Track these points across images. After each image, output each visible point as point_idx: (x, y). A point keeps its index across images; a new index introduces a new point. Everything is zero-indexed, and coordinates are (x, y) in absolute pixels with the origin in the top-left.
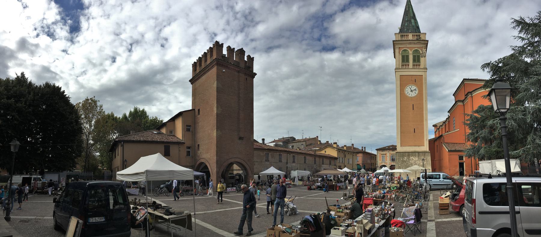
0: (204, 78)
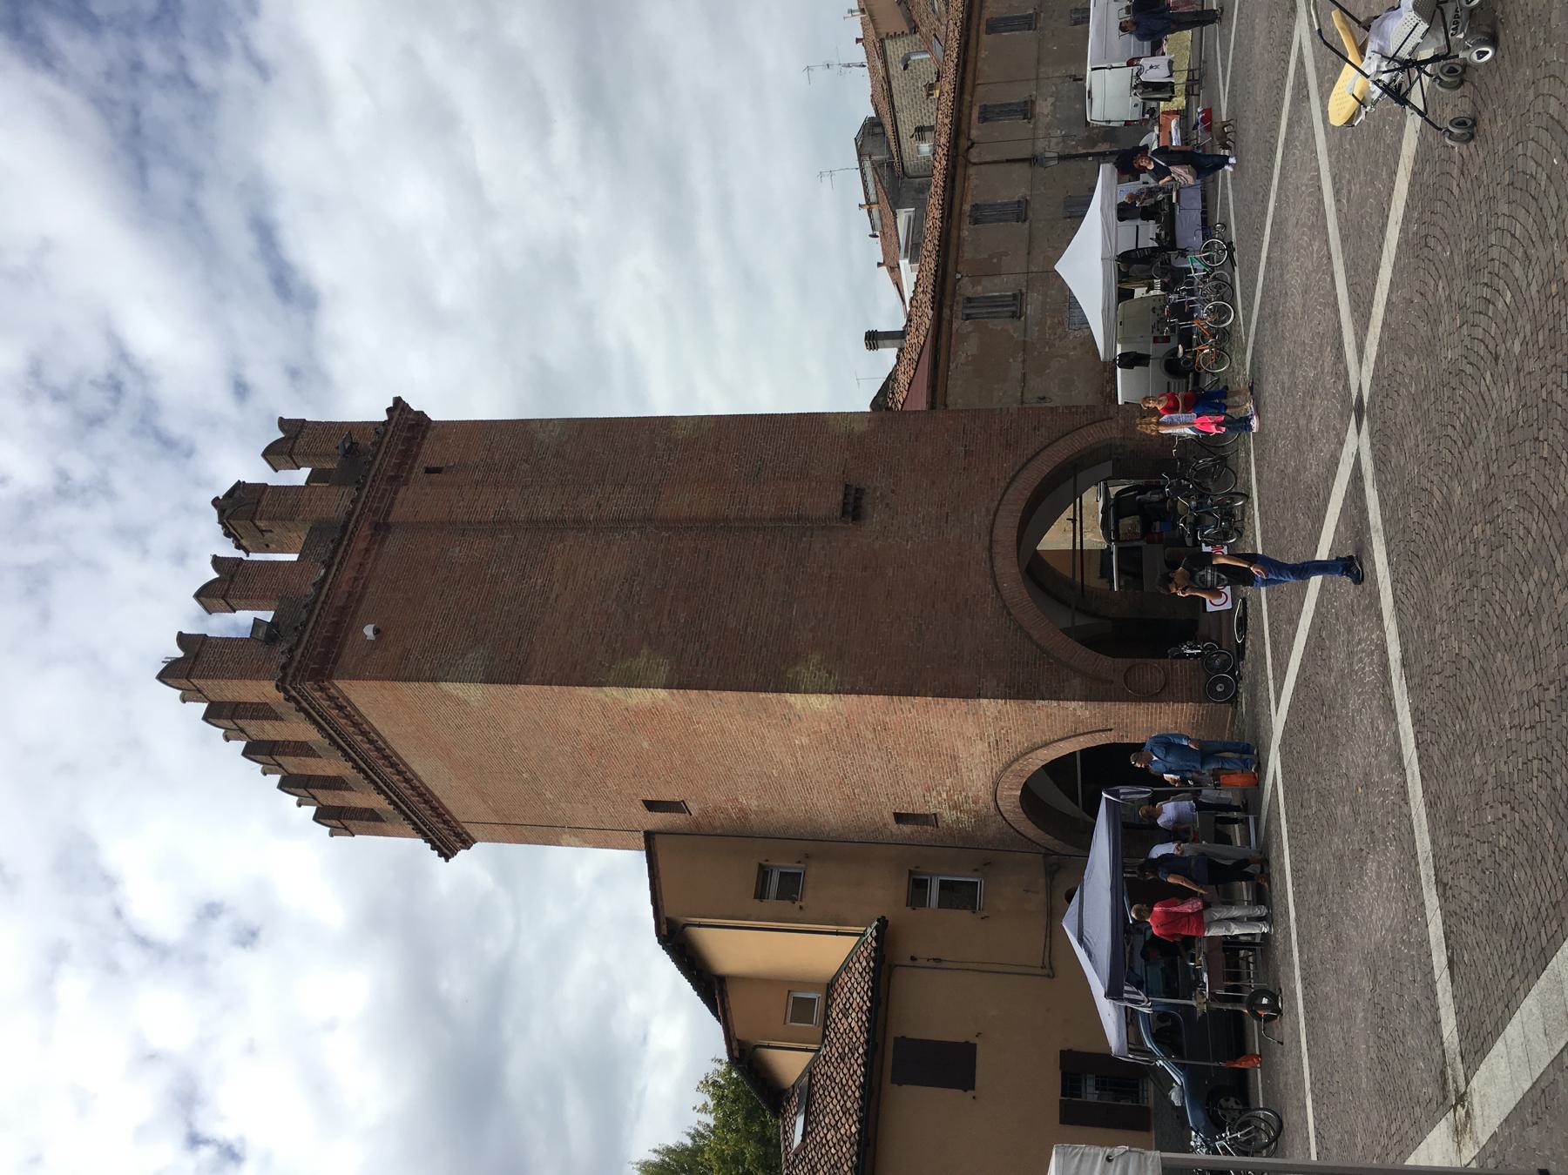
0: (424, 767)
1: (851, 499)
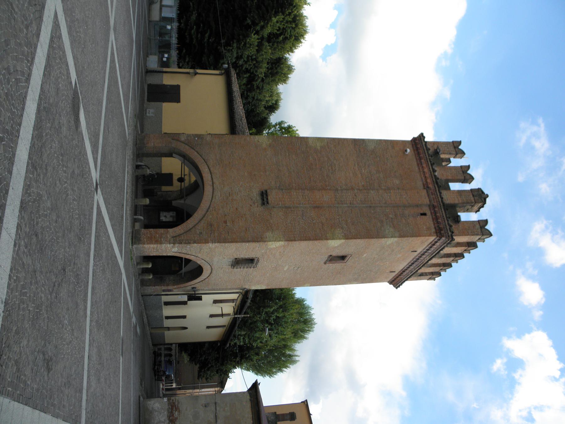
1: (265, 199)
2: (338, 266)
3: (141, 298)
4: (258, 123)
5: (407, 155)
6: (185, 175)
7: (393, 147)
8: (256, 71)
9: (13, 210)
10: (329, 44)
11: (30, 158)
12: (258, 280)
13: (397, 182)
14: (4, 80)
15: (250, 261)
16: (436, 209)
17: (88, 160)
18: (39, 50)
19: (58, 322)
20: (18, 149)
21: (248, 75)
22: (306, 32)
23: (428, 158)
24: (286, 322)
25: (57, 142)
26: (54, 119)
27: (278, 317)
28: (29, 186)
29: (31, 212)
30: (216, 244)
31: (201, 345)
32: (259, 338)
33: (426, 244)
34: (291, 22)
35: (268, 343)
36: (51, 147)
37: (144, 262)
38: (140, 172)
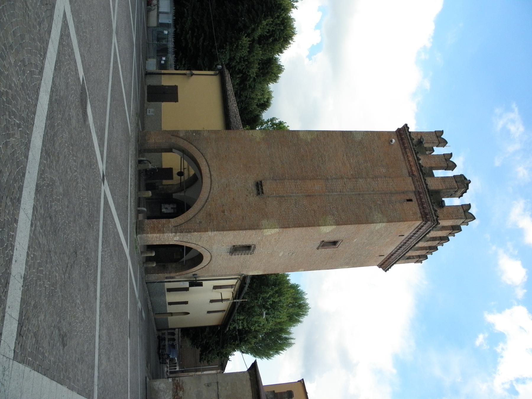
1: (260, 190)
2: (330, 251)
3: (145, 286)
4: (251, 120)
5: (393, 145)
6: (184, 169)
7: (379, 138)
8: (248, 72)
9: (30, 192)
10: (315, 44)
11: (44, 145)
12: (255, 266)
13: (384, 170)
14: (20, 71)
15: (248, 248)
16: (421, 195)
17: (95, 152)
18: (50, 46)
19: (71, 301)
20: (33, 136)
21: (241, 75)
22: (294, 33)
23: (414, 148)
24: (282, 307)
25: (67, 133)
26: (64, 111)
27: (274, 302)
28: (43, 171)
29: (46, 196)
30: (215, 232)
31: (202, 329)
32: (256, 322)
33: (413, 228)
34: (279, 24)
35: (265, 326)
36: (62, 136)
37: (147, 251)
38: (142, 167)
